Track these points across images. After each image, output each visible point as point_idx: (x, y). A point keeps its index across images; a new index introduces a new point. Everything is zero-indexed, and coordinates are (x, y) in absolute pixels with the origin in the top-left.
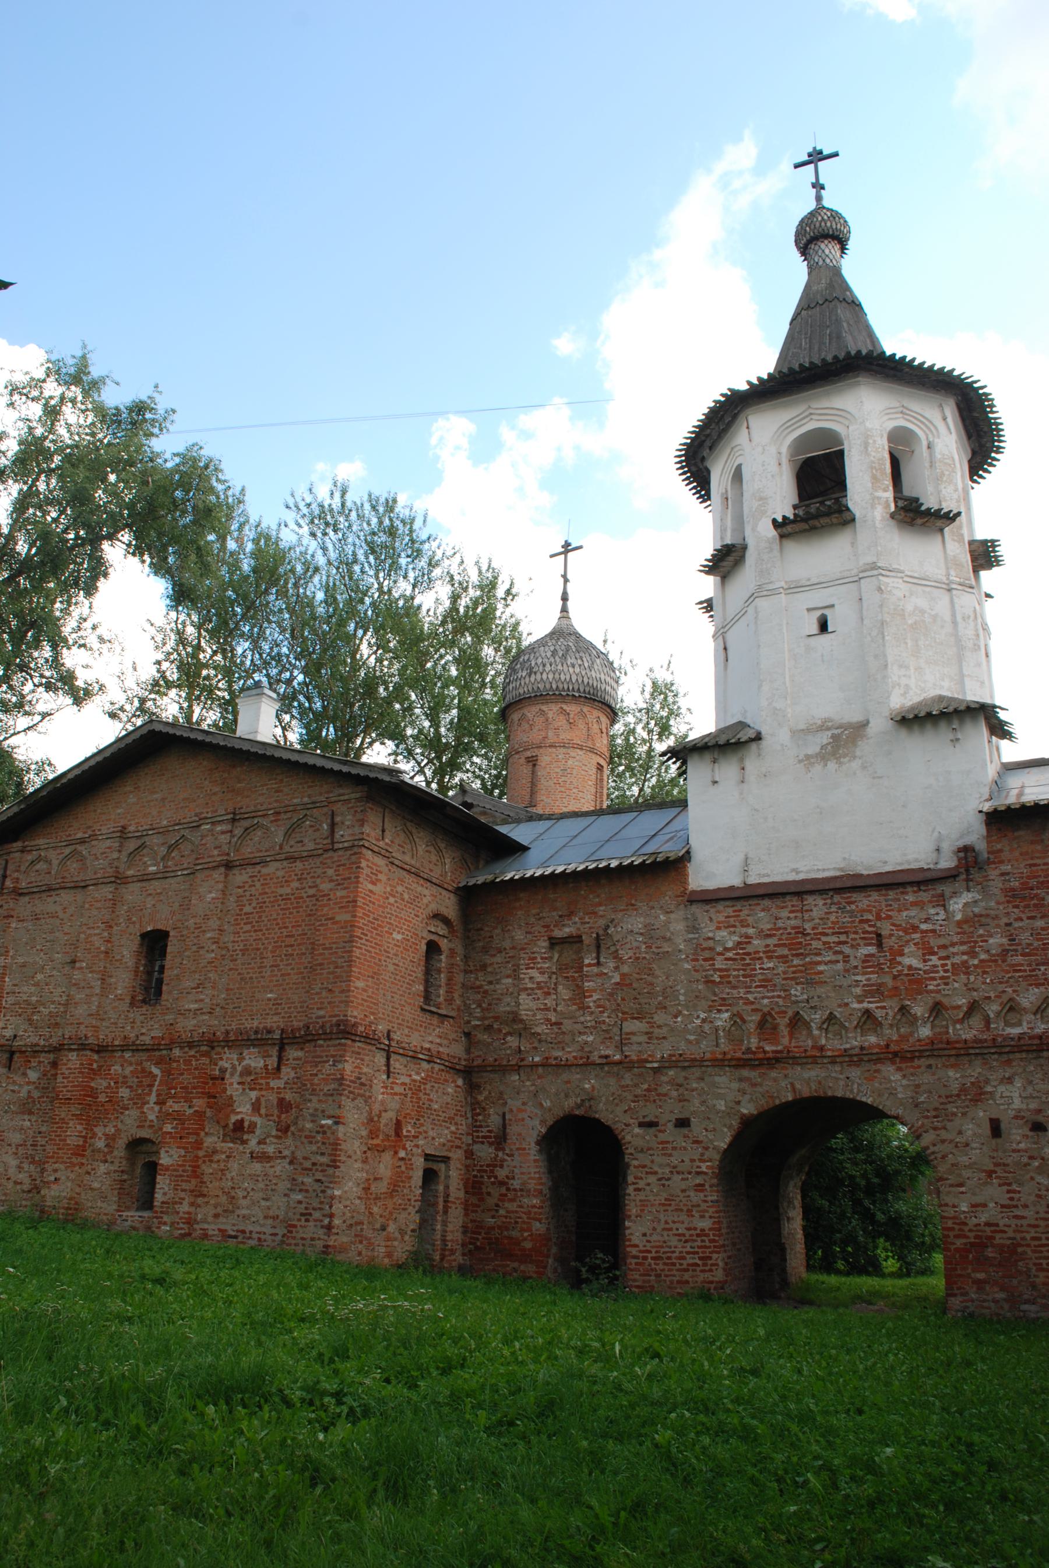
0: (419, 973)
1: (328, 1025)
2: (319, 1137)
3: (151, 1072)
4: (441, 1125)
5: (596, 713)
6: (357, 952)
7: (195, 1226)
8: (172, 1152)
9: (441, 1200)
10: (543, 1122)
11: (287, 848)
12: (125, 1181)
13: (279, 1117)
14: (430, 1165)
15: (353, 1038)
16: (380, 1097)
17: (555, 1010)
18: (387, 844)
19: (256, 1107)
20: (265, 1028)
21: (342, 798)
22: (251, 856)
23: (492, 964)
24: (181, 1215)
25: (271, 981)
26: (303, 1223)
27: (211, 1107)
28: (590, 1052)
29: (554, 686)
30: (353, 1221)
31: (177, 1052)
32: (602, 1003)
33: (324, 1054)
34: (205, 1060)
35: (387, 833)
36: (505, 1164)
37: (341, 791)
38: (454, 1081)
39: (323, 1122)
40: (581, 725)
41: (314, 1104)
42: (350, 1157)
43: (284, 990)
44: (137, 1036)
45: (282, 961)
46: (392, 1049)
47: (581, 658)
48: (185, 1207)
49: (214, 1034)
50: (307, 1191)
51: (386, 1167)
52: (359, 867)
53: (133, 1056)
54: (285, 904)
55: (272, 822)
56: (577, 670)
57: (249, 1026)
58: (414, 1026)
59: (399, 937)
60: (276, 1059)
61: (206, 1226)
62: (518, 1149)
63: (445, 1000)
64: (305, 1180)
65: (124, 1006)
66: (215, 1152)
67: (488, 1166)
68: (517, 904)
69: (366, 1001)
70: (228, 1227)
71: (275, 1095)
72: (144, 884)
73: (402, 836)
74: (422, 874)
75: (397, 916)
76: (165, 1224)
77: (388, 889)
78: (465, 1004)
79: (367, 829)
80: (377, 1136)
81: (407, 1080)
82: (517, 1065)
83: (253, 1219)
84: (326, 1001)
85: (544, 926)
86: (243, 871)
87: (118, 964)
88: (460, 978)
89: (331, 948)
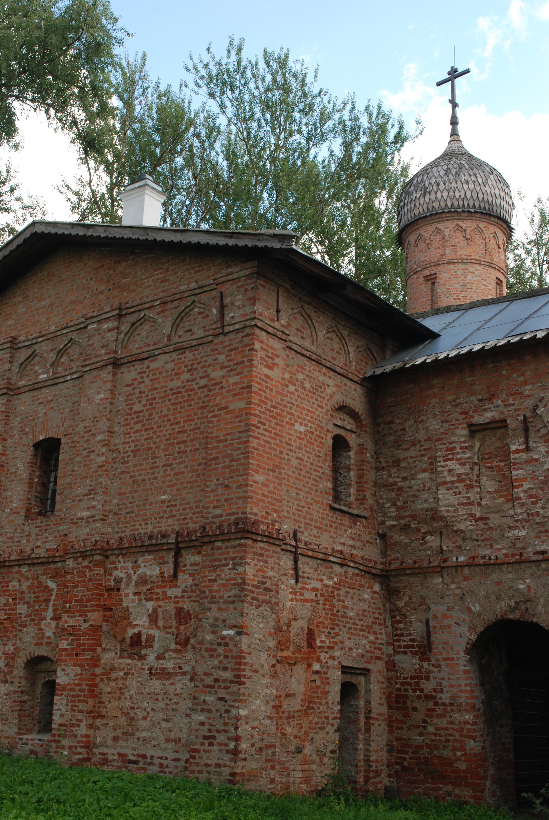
0: (327, 468)
1: (226, 525)
2: (220, 650)
3: (47, 587)
4: (359, 635)
5: (492, 229)
6: (254, 443)
7: (95, 750)
8: (68, 670)
9: (362, 717)
10: (472, 628)
11: (175, 339)
12: (25, 702)
13: (178, 629)
14: (348, 678)
15: (254, 537)
16: (289, 604)
17: (479, 504)
18: (282, 326)
19: (153, 618)
20: (160, 532)
21: (231, 277)
22: (139, 351)
23: (404, 459)
24: (79, 738)
25: (164, 482)
26: (206, 747)
27: (107, 621)
28: (523, 548)
29: (449, 204)
30: (262, 745)
31: (70, 563)
32: (534, 492)
33: (222, 557)
34: (99, 570)
35: (282, 313)
36: (431, 675)
37: (230, 270)
38: (371, 587)
39: (225, 633)
40: (478, 240)
41: (212, 614)
42: (256, 671)
43: (178, 490)
44: (33, 549)
45: (175, 459)
46: (299, 551)
47: (475, 175)
48: (82, 730)
49: (108, 542)
50: (209, 711)
51: (299, 682)
52: (252, 349)
53: (30, 571)
54: (176, 398)
55: (158, 313)
56: (472, 186)
57: (143, 532)
58: (323, 527)
59: (302, 429)
60: (172, 565)
61: (105, 750)
62: (445, 659)
63: (357, 500)
64: (207, 698)
65: (20, 519)
66: (112, 669)
67: (412, 678)
68: (431, 392)
69: (267, 497)
70: (128, 752)
71: (172, 605)
72: (35, 393)
73: (300, 320)
74: (324, 362)
75: (298, 406)
76: (63, 748)
77: (287, 376)
78: (378, 504)
79: (259, 308)
80: (287, 648)
81: (318, 585)
82: (439, 566)
83: (154, 743)
84: (222, 498)
85: (461, 413)
86: (132, 369)
87: (13, 476)
88: (371, 476)
89: (226, 440)
